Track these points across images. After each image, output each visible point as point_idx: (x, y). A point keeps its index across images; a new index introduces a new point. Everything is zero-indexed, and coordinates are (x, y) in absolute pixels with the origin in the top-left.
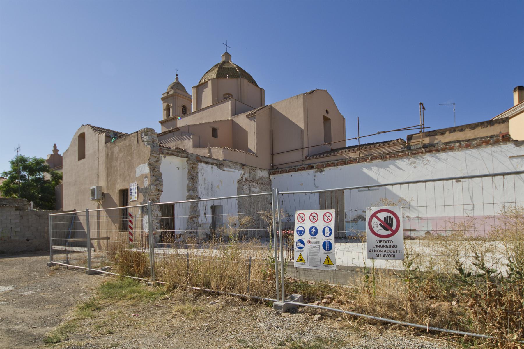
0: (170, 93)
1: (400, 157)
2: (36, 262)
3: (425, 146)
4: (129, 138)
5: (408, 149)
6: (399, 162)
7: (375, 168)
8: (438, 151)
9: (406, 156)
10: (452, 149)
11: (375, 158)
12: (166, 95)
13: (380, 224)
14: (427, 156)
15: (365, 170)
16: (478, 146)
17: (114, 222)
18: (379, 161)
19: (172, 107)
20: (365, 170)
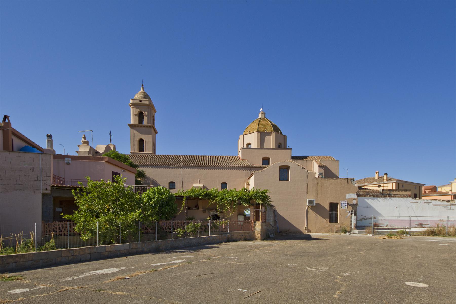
0: (143, 102)
1: (379, 197)
2: (269, 245)
3: (388, 194)
4: (339, 180)
5: (152, 166)
6: (379, 199)
7: (370, 200)
8: (392, 197)
9: (381, 197)
10: (396, 197)
11: (370, 196)
12: (138, 102)
13: (242, 251)
14: (388, 198)
15: (366, 200)
16: (403, 197)
17: (324, 218)
18: (372, 197)
19: (146, 115)
20: (366, 200)
